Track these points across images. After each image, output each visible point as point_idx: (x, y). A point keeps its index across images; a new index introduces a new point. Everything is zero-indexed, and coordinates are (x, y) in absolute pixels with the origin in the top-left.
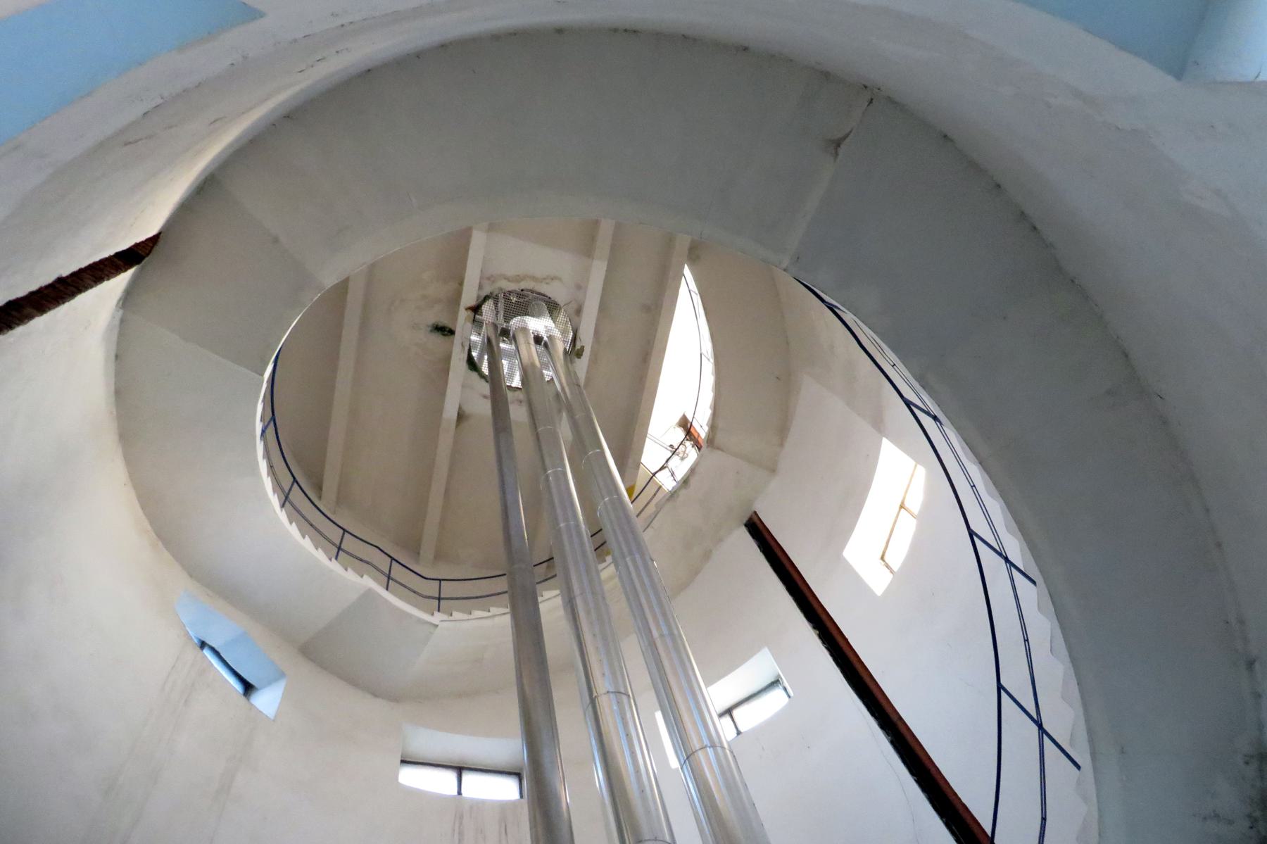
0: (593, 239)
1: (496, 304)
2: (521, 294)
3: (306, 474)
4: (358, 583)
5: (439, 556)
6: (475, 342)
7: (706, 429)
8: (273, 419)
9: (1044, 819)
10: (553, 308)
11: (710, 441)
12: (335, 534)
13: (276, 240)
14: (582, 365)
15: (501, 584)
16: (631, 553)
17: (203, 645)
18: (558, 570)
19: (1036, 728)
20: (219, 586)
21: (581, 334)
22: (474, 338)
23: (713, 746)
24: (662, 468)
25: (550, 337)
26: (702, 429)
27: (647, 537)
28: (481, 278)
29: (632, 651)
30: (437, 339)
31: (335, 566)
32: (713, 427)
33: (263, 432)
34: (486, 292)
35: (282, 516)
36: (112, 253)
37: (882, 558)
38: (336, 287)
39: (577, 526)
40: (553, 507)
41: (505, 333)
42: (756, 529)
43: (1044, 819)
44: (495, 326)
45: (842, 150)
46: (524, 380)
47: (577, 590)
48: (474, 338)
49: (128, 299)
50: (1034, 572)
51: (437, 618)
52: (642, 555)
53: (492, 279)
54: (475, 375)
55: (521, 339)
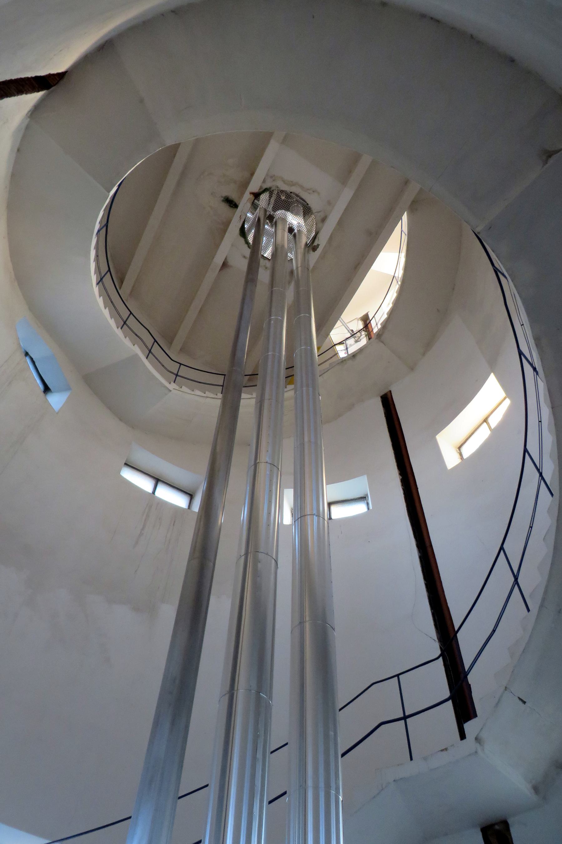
0: (350, 172)
1: (270, 197)
2: (289, 195)
3: (115, 272)
4: (131, 348)
5: (182, 350)
6: (249, 218)
7: (379, 326)
8: (107, 225)
9: (494, 631)
10: (307, 211)
11: (379, 335)
12: (125, 313)
13: (142, 101)
14: (314, 257)
15: (220, 380)
16: (308, 386)
17: (27, 354)
18: (259, 383)
19: (513, 579)
20: (45, 320)
21: (320, 236)
22: (249, 215)
23: (318, 516)
24: (341, 343)
25: (299, 231)
26: (376, 326)
27: (320, 380)
28: (267, 175)
29: (289, 446)
30: (225, 208)
31: (119, 332)
32: (385, 325)
33: (99, 231)
34: (265, 186)
35: (96, 289)
36: (33, 76)
37: (460, 448)
38: (170, 147)
39: (280, 357)
40: (268, 339)
41: (271, 218)
42: (388, 402)
43: (494, 631)
44: (265, 211)
45: (551, 161)
46: (274, 255)
47: (267, 396)
48: (249, 215)
49: (37, 109)
50: (556, 490)
51: (172, 386)
52: (314, 389)
53: (273, 178)
54: (242, 240)
55: (280, 226)
